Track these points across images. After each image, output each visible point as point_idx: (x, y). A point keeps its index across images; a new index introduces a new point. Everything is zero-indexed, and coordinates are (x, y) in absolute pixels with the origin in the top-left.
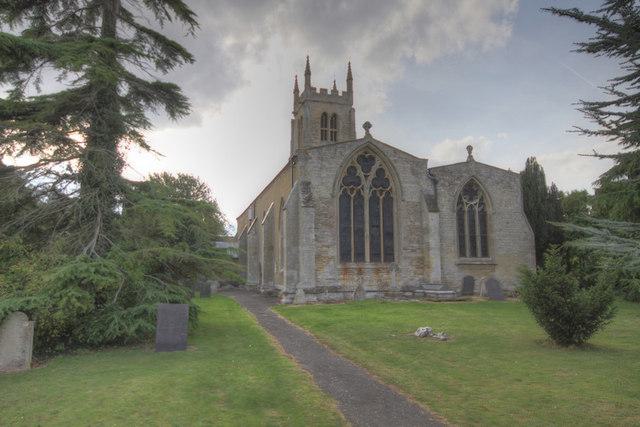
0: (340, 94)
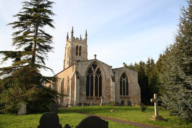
0: (83, 40)
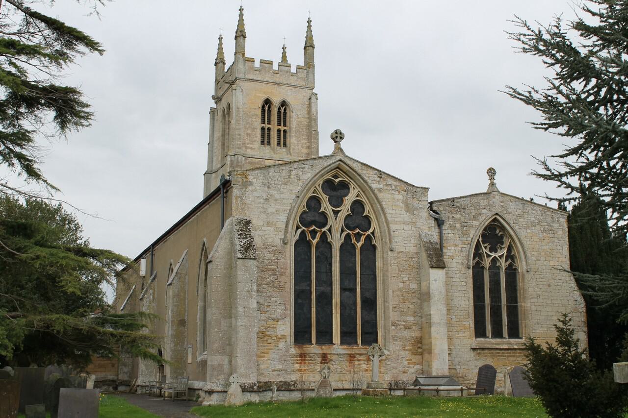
0: (293, 70)
